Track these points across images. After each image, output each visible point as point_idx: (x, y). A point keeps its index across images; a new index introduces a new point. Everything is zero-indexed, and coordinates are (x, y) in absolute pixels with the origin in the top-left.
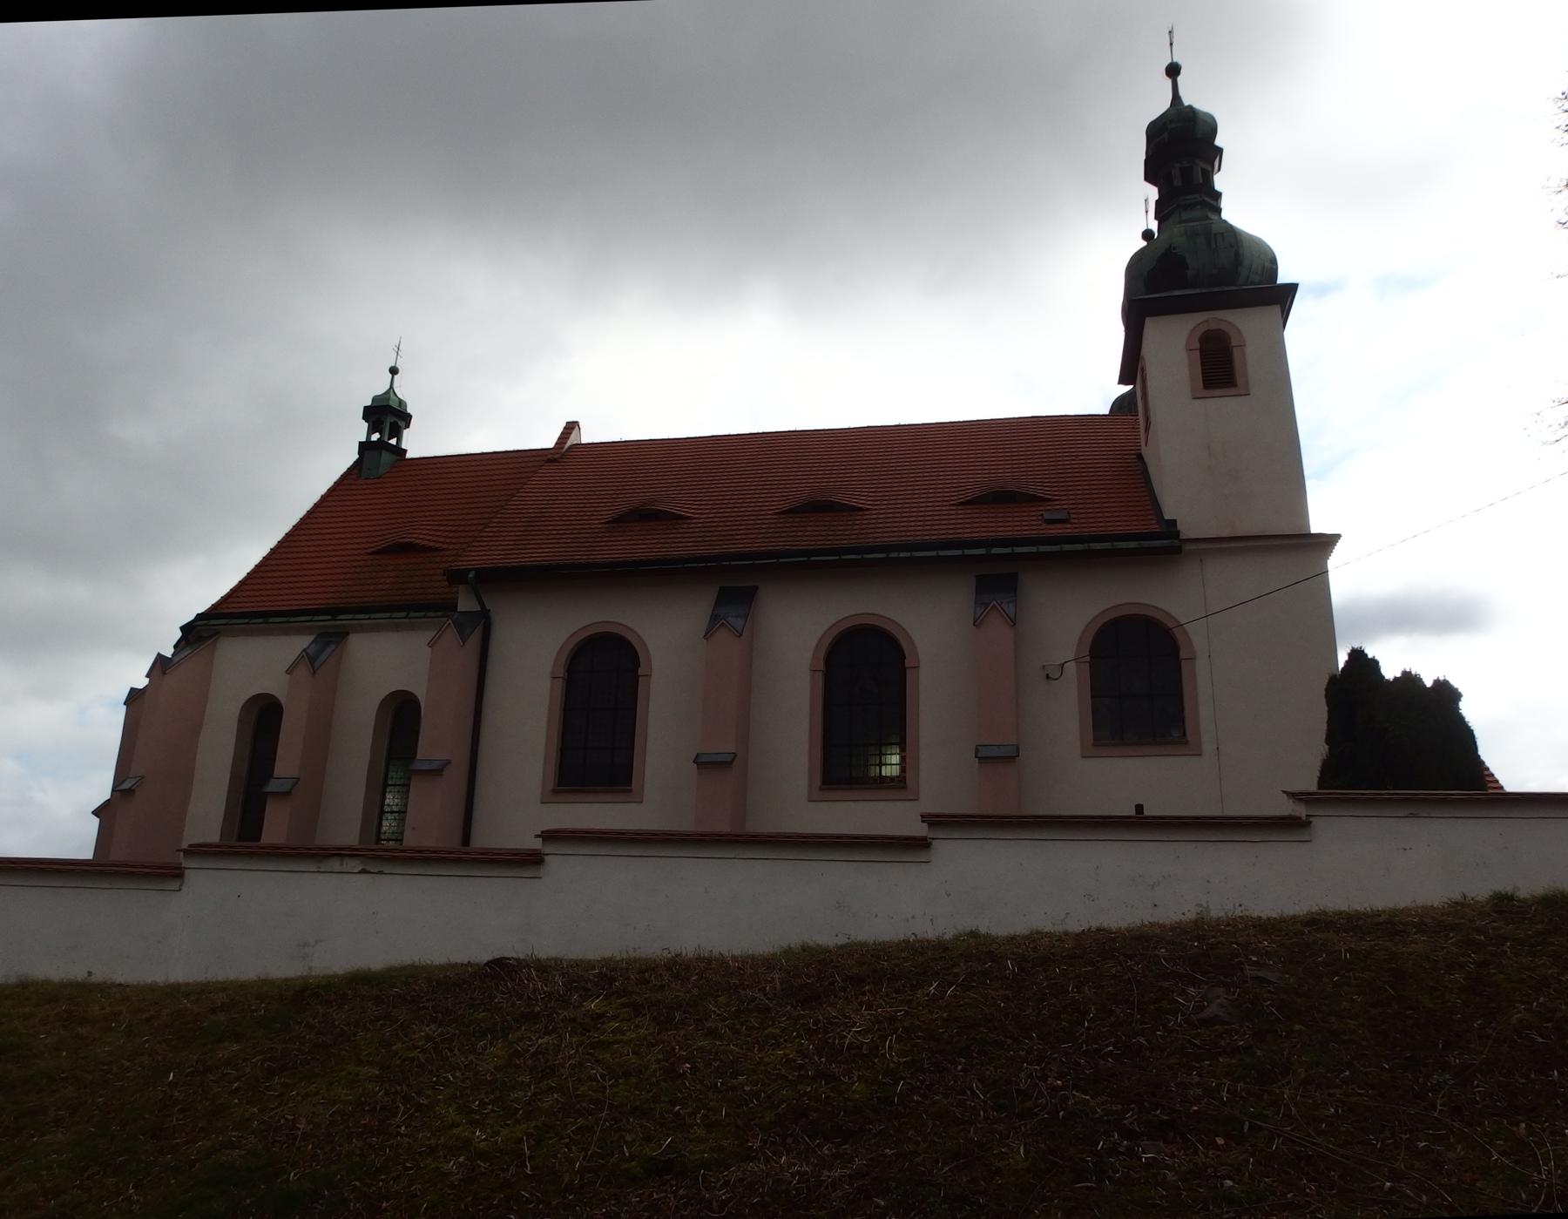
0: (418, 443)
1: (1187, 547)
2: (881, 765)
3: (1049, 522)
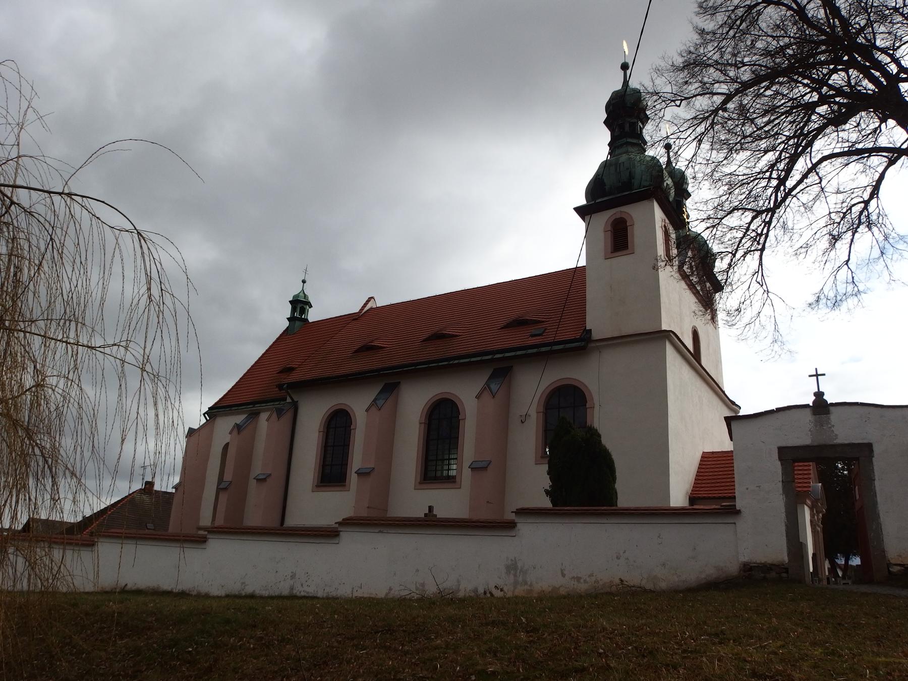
0: (313, 315)
1: (593, 345)
2: (448, 470)
3: (533, 336)
